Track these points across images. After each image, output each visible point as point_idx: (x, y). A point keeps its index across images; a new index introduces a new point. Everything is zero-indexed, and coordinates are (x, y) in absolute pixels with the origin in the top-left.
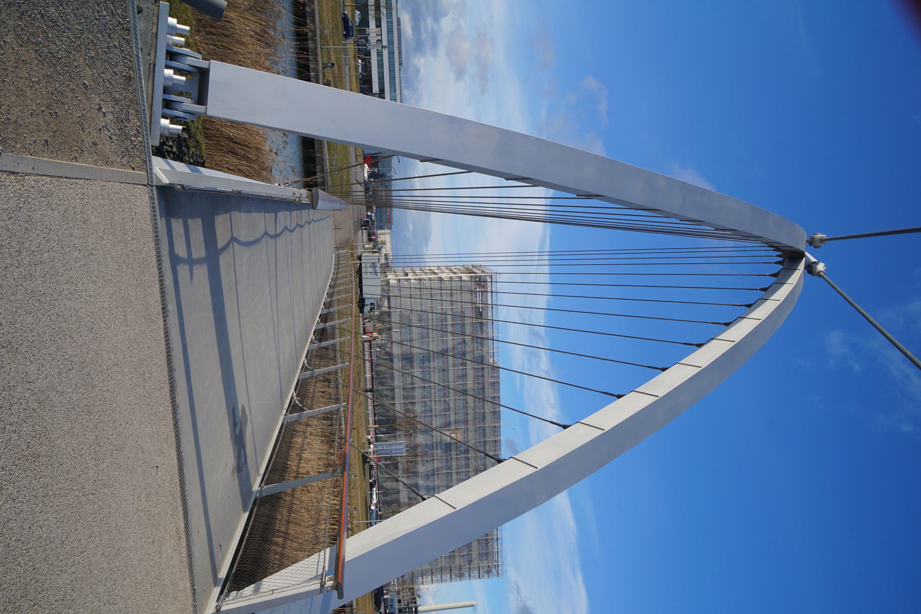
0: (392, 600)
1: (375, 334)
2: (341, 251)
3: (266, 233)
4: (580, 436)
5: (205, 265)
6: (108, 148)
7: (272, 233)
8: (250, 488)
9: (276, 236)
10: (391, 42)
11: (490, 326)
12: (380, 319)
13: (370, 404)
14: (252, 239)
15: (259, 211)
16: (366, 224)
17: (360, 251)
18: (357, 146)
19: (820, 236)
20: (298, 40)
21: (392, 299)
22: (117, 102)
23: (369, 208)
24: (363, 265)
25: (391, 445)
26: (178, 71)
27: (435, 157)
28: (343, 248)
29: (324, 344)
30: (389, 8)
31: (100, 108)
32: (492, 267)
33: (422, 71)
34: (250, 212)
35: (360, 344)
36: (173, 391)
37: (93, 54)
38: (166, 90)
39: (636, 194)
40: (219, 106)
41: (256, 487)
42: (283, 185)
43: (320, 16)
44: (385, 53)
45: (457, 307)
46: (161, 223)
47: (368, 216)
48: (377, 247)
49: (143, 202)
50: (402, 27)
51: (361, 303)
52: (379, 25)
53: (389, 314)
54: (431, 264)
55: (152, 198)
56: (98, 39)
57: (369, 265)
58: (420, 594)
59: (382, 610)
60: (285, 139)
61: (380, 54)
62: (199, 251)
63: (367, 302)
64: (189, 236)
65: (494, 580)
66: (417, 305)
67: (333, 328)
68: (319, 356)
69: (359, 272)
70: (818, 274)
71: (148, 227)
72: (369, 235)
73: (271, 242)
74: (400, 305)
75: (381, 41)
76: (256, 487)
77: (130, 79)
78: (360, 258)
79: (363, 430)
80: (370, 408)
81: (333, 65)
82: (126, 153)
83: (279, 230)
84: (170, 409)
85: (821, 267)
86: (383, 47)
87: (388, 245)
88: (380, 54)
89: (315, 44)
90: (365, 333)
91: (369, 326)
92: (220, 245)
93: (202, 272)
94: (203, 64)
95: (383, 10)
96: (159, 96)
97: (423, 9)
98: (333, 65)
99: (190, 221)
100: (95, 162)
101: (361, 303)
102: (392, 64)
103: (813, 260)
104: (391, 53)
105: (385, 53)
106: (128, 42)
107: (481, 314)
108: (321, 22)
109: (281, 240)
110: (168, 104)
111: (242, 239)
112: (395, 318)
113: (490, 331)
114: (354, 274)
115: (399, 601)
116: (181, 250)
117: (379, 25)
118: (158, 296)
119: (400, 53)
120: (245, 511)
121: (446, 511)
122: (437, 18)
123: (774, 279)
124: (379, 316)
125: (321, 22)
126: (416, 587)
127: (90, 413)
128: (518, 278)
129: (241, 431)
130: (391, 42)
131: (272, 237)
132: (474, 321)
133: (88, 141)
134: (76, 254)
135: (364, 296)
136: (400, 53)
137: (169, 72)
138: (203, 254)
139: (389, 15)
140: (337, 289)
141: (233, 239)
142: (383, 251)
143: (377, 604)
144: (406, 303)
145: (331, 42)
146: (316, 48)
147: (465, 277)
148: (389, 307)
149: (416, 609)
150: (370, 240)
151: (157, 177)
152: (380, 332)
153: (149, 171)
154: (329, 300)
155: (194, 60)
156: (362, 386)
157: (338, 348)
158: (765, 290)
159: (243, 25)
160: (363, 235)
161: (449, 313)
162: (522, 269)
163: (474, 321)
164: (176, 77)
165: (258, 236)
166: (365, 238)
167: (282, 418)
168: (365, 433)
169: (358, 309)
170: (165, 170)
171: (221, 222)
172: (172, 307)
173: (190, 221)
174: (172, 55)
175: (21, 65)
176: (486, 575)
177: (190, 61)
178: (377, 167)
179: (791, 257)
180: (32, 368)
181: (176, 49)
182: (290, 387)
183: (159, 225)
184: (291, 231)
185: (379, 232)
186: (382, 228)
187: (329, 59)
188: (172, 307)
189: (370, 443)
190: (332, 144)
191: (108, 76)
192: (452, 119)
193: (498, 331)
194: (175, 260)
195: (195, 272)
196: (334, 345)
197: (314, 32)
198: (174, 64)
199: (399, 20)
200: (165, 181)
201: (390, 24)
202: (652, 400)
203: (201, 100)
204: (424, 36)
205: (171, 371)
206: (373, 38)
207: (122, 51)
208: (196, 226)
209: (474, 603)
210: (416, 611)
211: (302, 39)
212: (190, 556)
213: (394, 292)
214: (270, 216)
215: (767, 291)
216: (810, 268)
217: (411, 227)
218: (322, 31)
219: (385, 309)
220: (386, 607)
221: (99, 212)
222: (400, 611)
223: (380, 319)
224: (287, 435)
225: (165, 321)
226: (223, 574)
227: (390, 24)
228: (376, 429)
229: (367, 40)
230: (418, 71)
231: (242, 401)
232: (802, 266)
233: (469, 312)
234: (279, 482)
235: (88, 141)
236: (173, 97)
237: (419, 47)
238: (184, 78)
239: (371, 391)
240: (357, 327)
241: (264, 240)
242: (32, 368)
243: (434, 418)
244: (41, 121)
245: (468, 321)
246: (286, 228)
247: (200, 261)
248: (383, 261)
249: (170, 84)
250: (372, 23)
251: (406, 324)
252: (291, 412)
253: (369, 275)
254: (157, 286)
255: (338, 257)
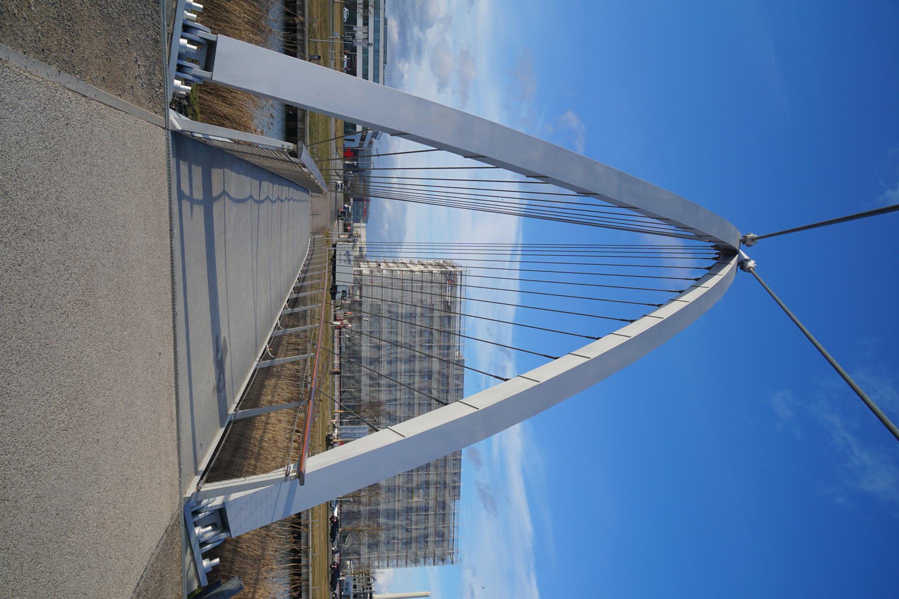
0: (348, 584)
1: (345, 322)
2: (316, 236)
3: (251, 196)
4: (517, 386)
5: (202, 207)
6: (140, 92)
7: (257, 198)
8: (227, 411)
9: (259, 202)
10: (377, 40)
11: (457, 320)
12: (350, 308)
13: (336, 390)
14: (240, 198)
15: (247, 175)
16: (341, 215)
17: (335, 239)
18: (337, 117)
19: (752, 235)
20: (286, 30)
21: (364, 288)
22: (148, 58)
23: (346, 199)
24: (337, 253)
25: (354, 429)
26: (191, 42)
27: (403, 130)
28: (319, 233)
29: (296, 310)
30: (377, 8)
31: (137, 61)
32: (462, 260)
33: (406, 76)
34: (239, 173)
35: (330, 330)
36: (173, 299)
37: (134, 18)
38: (180, 56)
39: (578, 177)
40: (221, 74)
41: (231, 411)
42: (271, 140)
43: (309, 11)
44: (371, 50)
45: (427, 299)
46: (173, 161)
47: (345, 208)
48: (352, 238)
49: (162, 140)
50: (388, 27)
51: (334, 290)
52: (366, 24)
53: (360, 303)
54: (404, 256)
55: (167, 140)
56: (137, 7)
57: (343, 253)
58: (376, 577)
59: (337, 591)
60: (272, 120)
61: (365, 52)
62: (198, 195)
63: (340, 289)
64: (192, 178)
65: (447, 567)
66: (388, 294)
67: (305, 297)
68: (292, 318)
69: (333, 260)
70: (749, 270)
71: (164, 162)
72: (345, 225)
73: (255, 206)
74: (371, 295)
75: (367, 39)
76: (231, 411)
77: (157, 41)
78: (334, 246)
79: (328, 413)
80: (337, 393)
81: (319, 57)
82: (151, 99)
83: (262, 198)
84: (171, 312)
85: (751, 264)
86: (369, 44)
87: (363, 239)
88: (365, 52)
89: (304, 36)
90: (335, 320)
91: (340, 313)
92: (215, 194)
93: (199, 211)
94: (212, 37)
95: (371, 9)
96: (174, 61)
97: (411, 17)
98: (319, 57)
99: (193, 166)
100: (132, 101)
101: (334, 290)
102: (376, 61)
103: (746, 257)
104: (376, 52)
105: (371, 50)
106: (157, 12)
107: (449, 308)
108: (310, 15)
109: (263, 206)
110: (180, 68)
111: (232, 195)
112: (366, 308)
113: (457, 324)
114: (328, 262)
115: (355, 587)
116: (185, 189)
117: (366, 24)
118: (168, 219)
119: (385, 52)
120: (221, 427)
121: (396, 438)
122: (424, 25)
123: (707, 271)
124: (350, 305)
125: (310, 15)
126: (372, 570)
127: (119, 289)
128: (487, 283)
129: (222, 358)
130: (377, 40)
131: (256, 201)
132: (443, 314)
133: (128, 86)
134: (117, 166)
135: (337, 283)
136: (385, 52)
137: (184, 41)
138: (201, 197)
139: (377, 14)
140: (309, 274)
141: (224, 193)
142: (358, 244)
143: (333, 584)
144: (377, 292)
145: (318, 36)
146: (304, 40)
147: (435, 270)
148: (361, 297)
149: (371, 595)
150: (345, 230)
151: (173, 124)
152: (350, 320)
153: (167, 117)
154: (303, 275)
155: (205, 33)
156: (330, 368)
157: (309, 313)
158: (697, 280)
159: (238, 11)
160: (339, 225)
161: (419, 305)
162: (493, 273)
163: (443, 314)
164: (189, 46)
165: (246, 196)
166: (341, 227)
167: (255, 363)
168: (330, 417)
169: (330, 295)
170: (177, 121)
171: (217, 174)
172: (176, 231)
173: (193, 166)
174: (186, 28)
175: (91, 20)
176: (441, 562)
177: (201, 34)
178: (357, 160)
179: (726, 253)
180: (88, 239)
181: (190, 23)
182: (264, 340)
183: (172, 163)
184: (273, 202)
185: (355, 224)
186: (358, 221)
187: (316, 51)
188: (176, 231)
189: (334, 427)
190: (314, 112)
191: (143, 37)
192: (419, 100)
193: (467, 325)
194: (181, 195)
195: (194, 210)
196: (305, 311)
197: (303, 23)
198: (187, 35)
199: (385, 20)
200: (179, 127)
201: (377, 23)
202: (583, 361)
203: (208, 67)
204: (410, 43)
205: (173, 283)
206: (359, 35)
207: (153, 19)
208: (197, 171)
209: (428, 593)
210: (371, 597)
211: (290, 28)
212: (179, 439)
213: (366, 281)
214: (256, 183)
215: (699, 281)
216: (742, 264)
217: (387, 226)
218: (310, 25)
219: (357, 298)
220: (341, 590)
221: (125, 144)
222: (355, 596)
223: (350, 308)
224: (263, 375)
225: (171, 241)
226: (202, 467)
227: (377, 23)
228: (341, 414)
229: (354, 37)
230: (402, 76)
231: (224, 334)
232: (734, 261)
233: (438, 306)
234: (252, 407)
235: (128, 86)
236: (186, 63)
237: (404, 53)
238: (195, 48)
239: (338, 373)
240: (327, 313)
241: (249, 202)
242: (88, 239)
243: (398, 406)
244: (101, 63)
245: (436, 314)
246: (268, 198)
247: (199, 202)
248: (358, 253)
249: (183, 51)
250: (360, 21)
251: (376, 315)
252: (265, 359)
253: (343, 263)
254: (168, 211)
255: (313, 242)
